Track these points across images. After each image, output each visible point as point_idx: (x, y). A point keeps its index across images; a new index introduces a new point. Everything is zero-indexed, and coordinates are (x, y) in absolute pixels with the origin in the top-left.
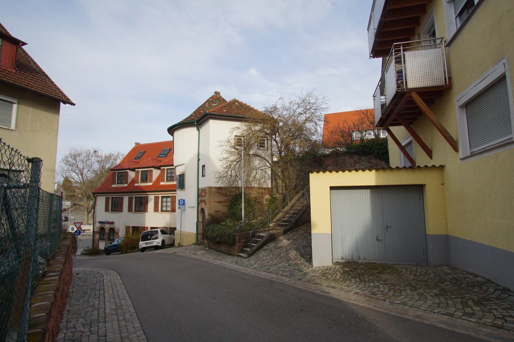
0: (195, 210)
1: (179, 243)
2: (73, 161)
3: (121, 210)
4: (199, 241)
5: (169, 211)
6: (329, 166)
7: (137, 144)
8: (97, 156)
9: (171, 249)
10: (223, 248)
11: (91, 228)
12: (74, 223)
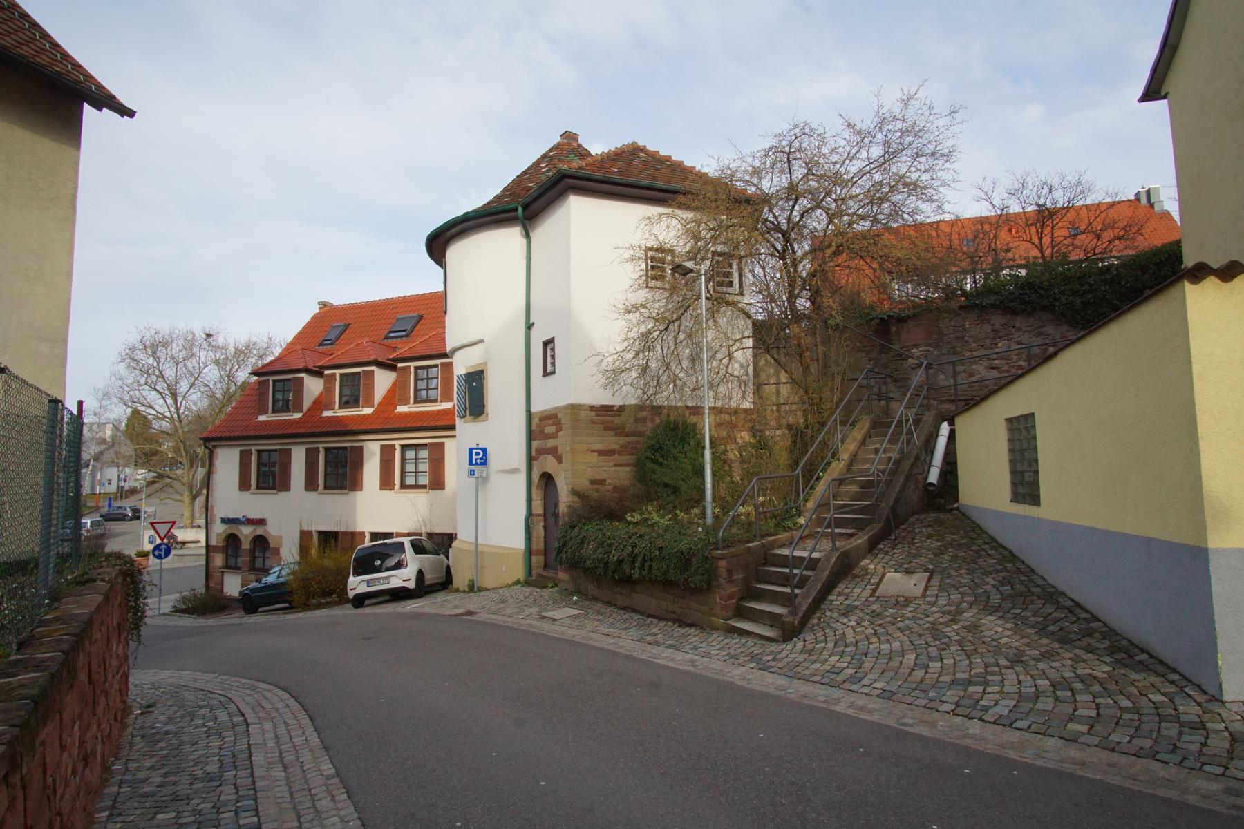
0: (522, 479)
1: (472, 581)
2: (151, 361)
3: (286, 486)
4: (534, 572)
5: (424, 487)
6: (915, 346)
7: (324, 305)
8: (216, 348)
9: (440, 597)
10: (640, 599)
11: (202, 536)
12: (152, 524)
